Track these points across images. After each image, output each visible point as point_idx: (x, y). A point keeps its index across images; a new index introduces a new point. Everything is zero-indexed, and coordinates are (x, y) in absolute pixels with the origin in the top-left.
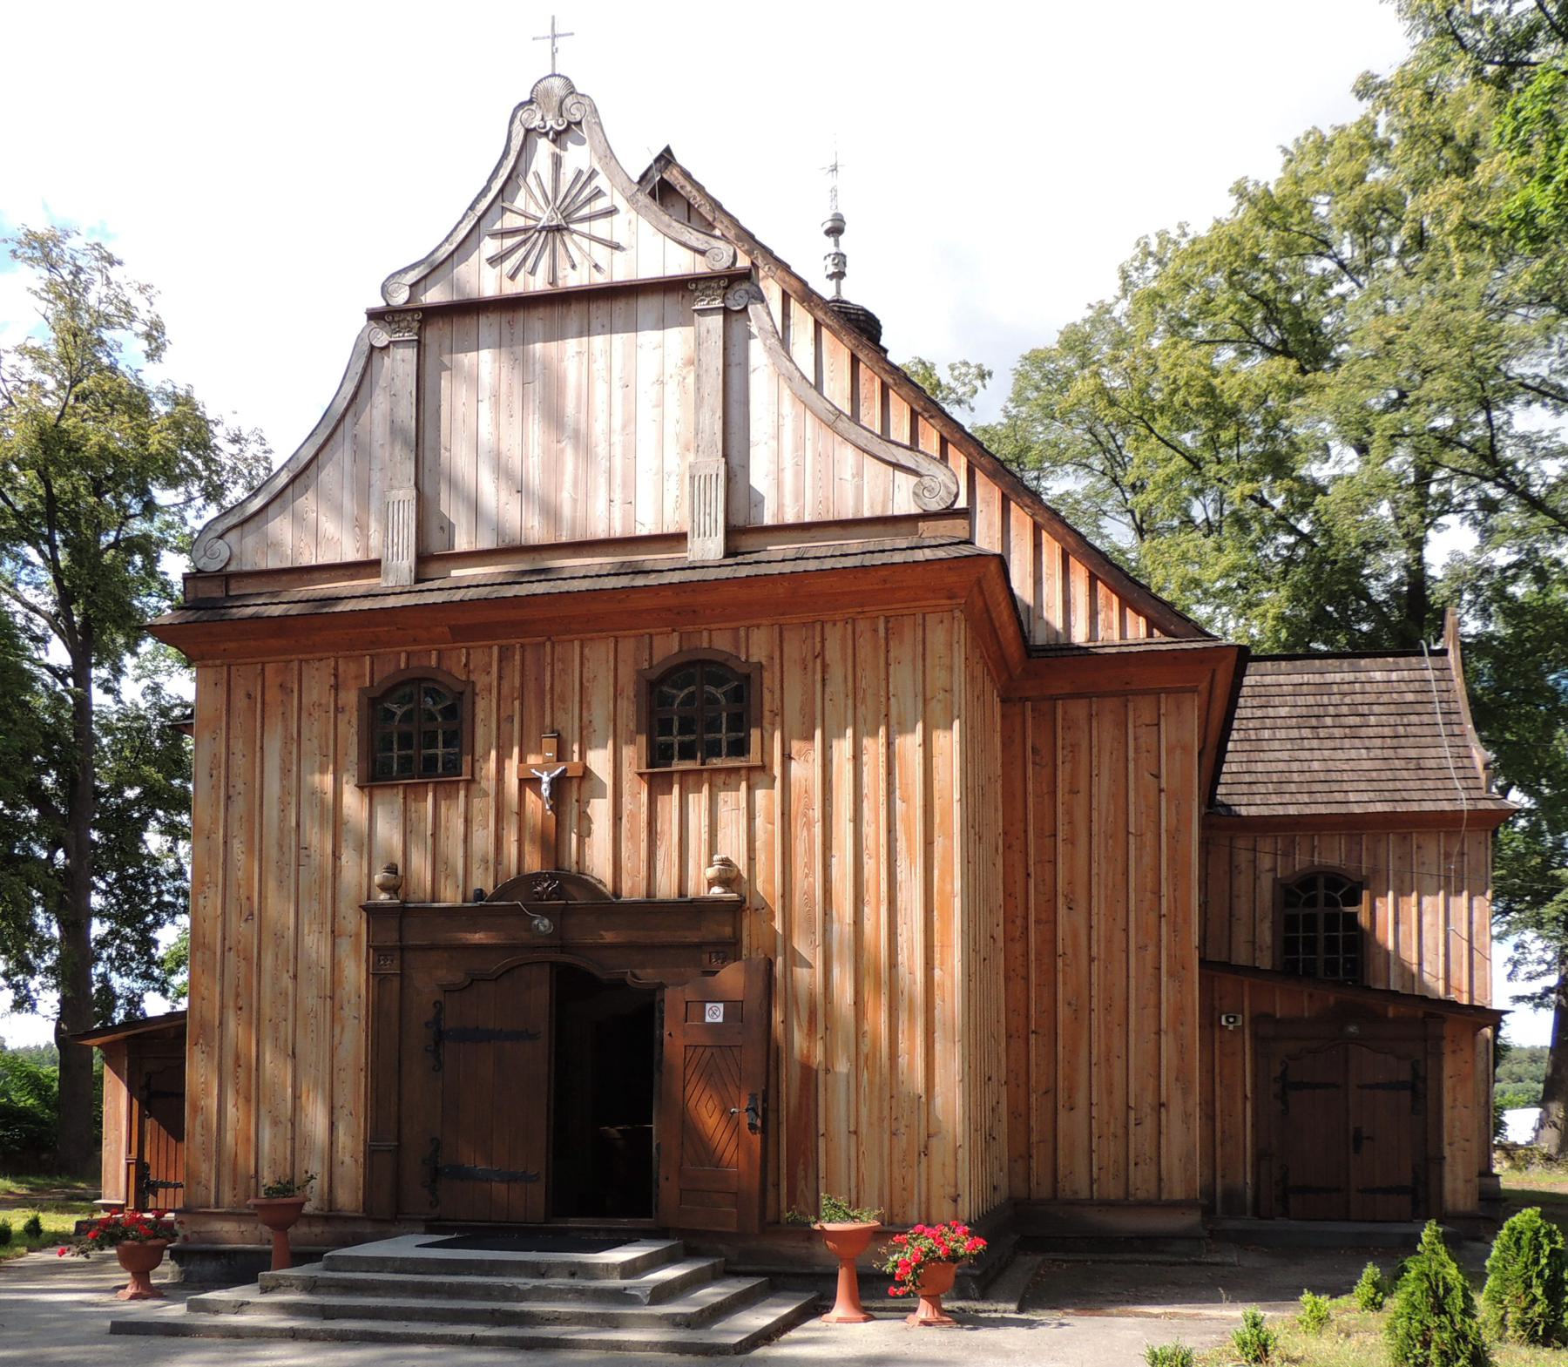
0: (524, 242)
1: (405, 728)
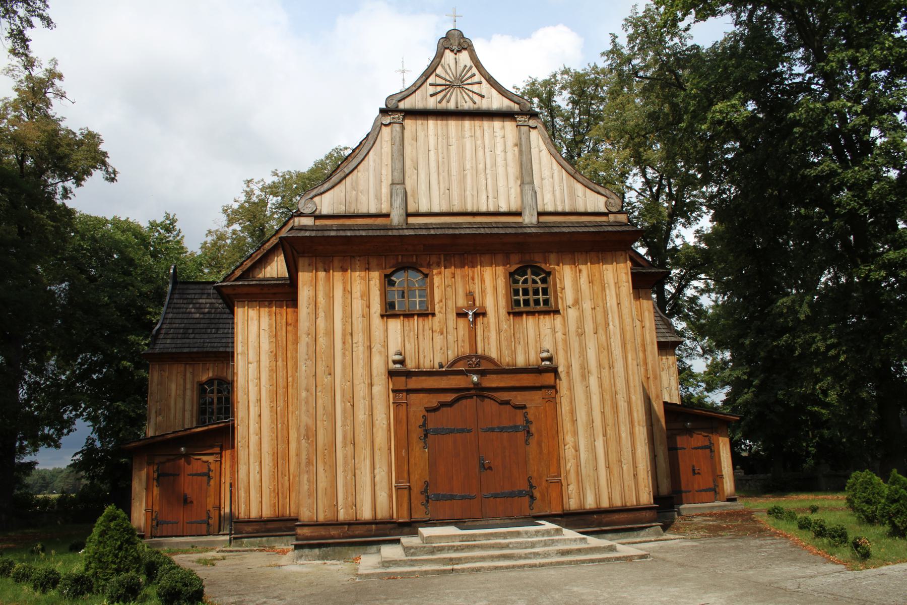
0: (445, 89)
1: (525, 286)
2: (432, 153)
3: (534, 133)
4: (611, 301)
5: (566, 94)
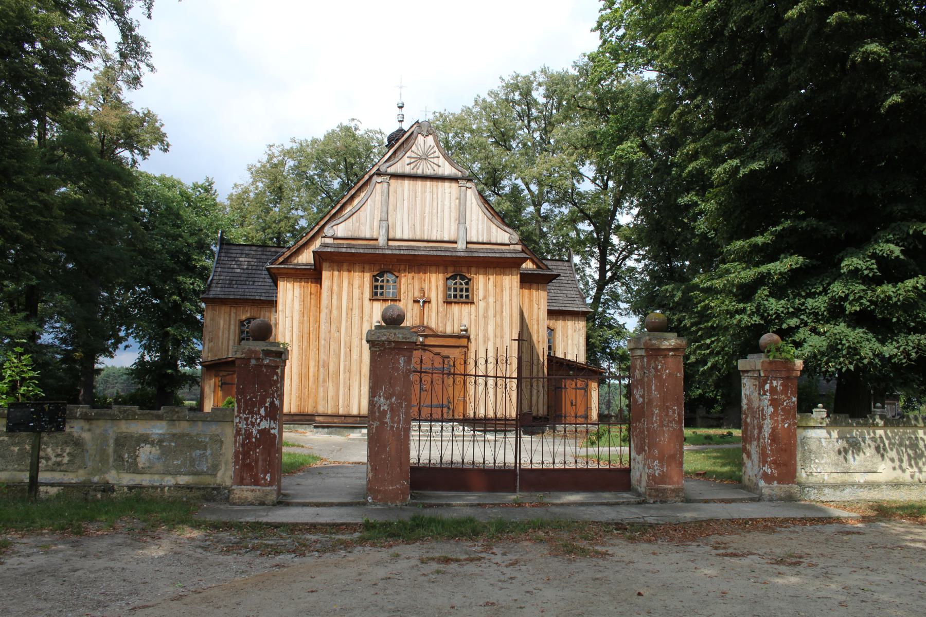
2: (406, 202)
3: (469, 191)
4: (506, 298)
5: (542, 90)
